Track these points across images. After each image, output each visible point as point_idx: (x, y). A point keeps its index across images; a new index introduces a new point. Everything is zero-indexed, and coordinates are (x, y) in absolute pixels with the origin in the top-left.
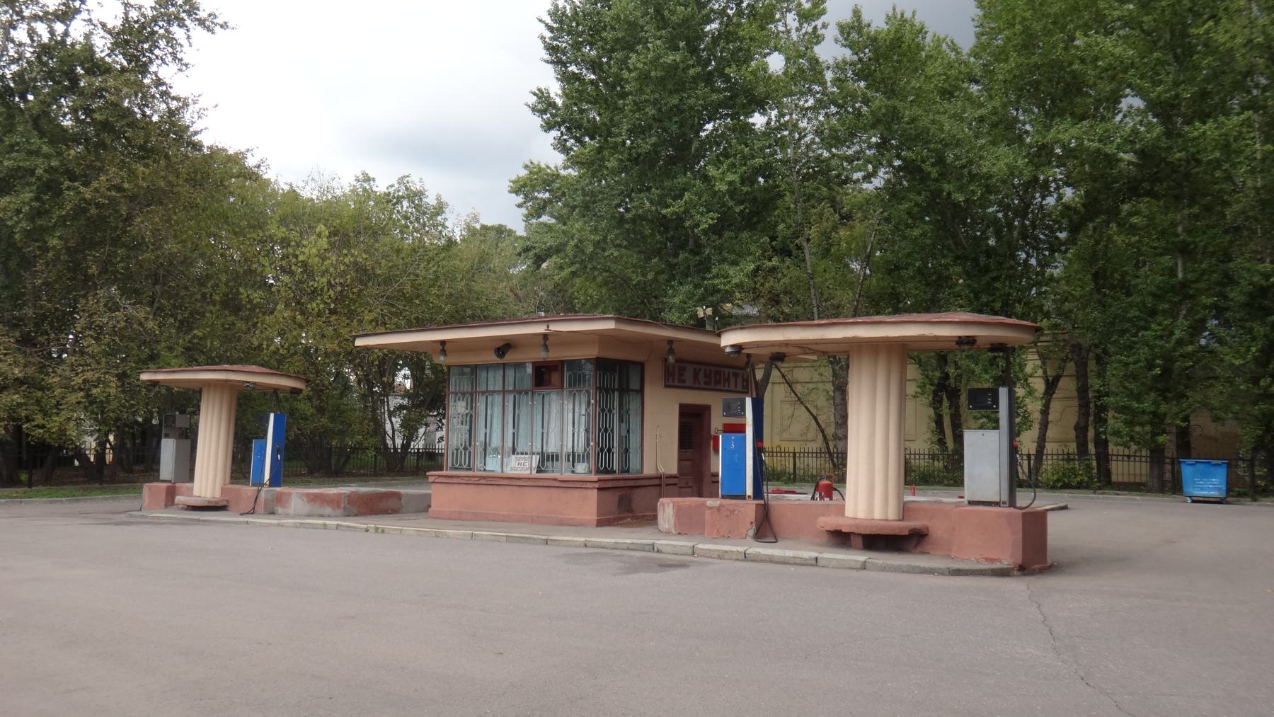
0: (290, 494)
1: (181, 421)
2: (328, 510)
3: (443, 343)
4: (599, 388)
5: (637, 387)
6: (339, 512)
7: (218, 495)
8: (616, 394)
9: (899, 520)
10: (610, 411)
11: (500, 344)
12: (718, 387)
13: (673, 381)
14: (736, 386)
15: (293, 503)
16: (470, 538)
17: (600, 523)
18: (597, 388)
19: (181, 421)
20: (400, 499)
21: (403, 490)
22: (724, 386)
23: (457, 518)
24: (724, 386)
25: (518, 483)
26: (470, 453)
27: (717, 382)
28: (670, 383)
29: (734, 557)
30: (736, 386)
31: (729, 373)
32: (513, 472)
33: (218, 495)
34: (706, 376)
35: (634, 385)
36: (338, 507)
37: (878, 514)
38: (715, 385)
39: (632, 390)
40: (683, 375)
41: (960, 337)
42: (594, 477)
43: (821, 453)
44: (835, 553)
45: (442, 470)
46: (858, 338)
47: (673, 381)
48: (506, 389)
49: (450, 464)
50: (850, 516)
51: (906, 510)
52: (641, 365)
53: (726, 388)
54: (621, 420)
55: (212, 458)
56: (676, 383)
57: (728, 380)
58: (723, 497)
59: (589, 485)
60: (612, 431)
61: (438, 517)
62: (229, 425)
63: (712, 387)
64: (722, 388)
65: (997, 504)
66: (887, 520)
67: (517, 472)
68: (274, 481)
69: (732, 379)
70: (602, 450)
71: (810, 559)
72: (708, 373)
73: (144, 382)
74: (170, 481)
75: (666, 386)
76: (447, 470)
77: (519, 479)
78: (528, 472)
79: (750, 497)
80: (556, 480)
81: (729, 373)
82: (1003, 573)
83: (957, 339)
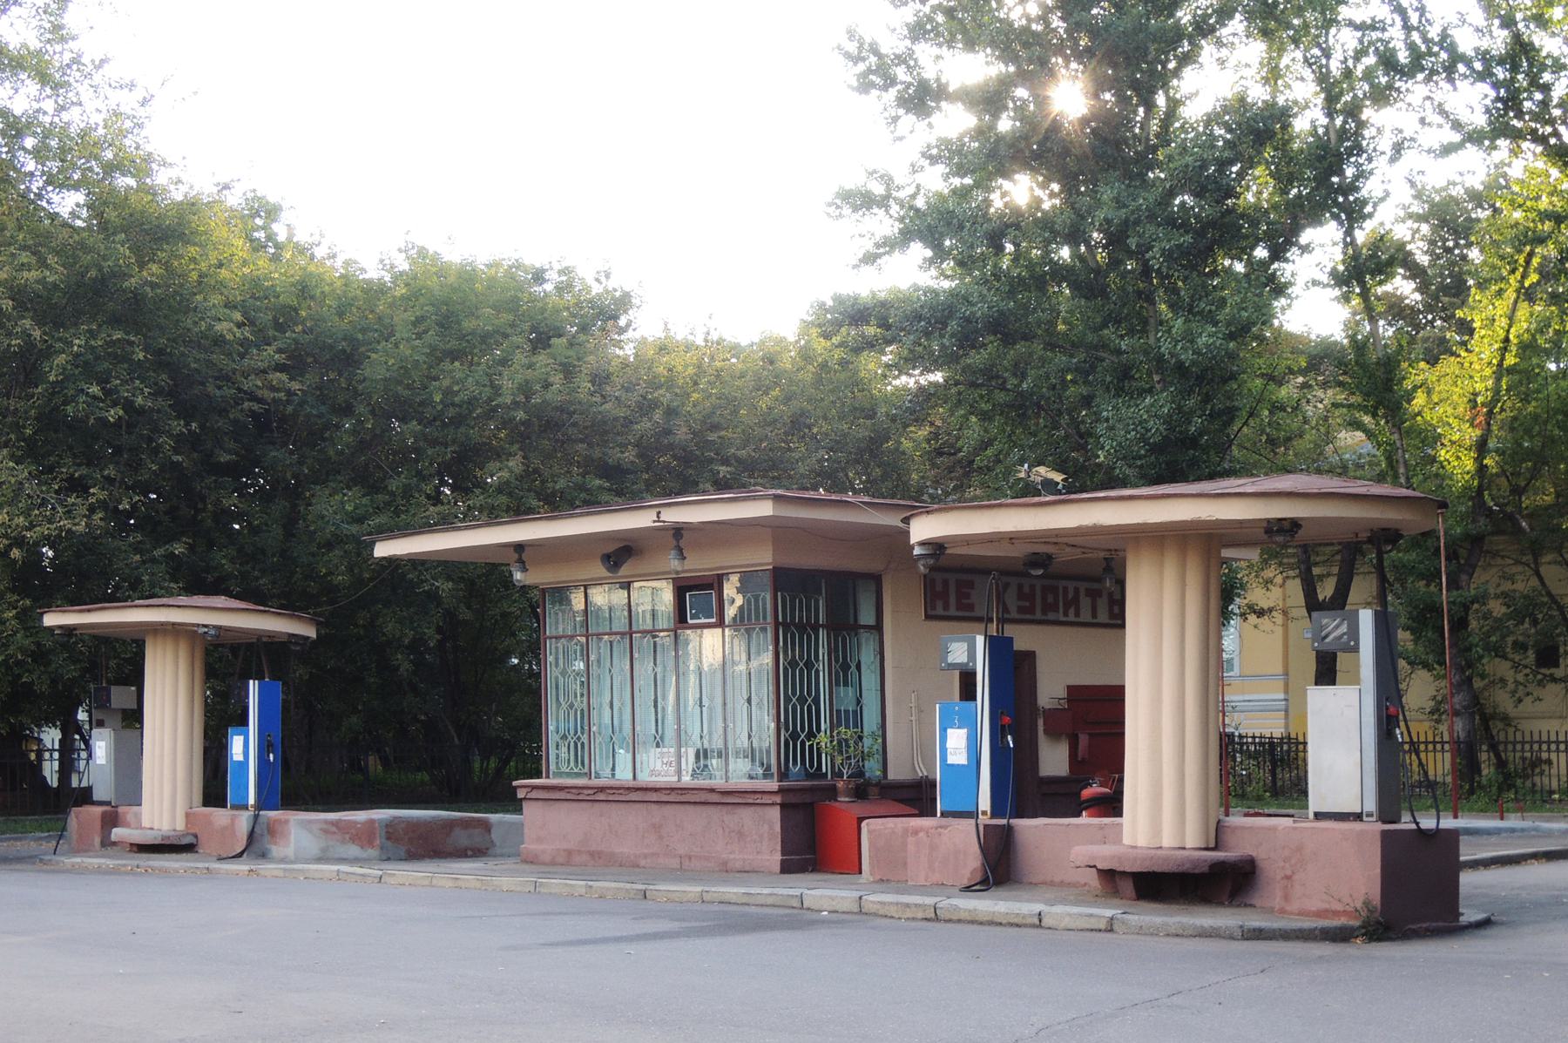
0: (287, 822)
1: (120, 697)
2: (354, 850)
3: (519, 547)
4: (786, 626)
5: (871, 621)
6: (372, 852)
7: (180, 825)
8: (822, 634)
9: (1207, 849)
10: (809, 665)
11: (611, 548)
12: (1051, 616)
13: (946, 607)
14: (1094, 615)
15: (292, 838)
16: (641, 897)
17: (787, 868)
18: (777, 624)
19: (120, 697)
20: (489, 831)
21: (494, 817)
22: (1066, 614)
23: (565, 862)
24: (1066, 614)
25: (654, 797)
26: (817, 672)
27: (1049, 607)
28: (940, 611)
29: (920, 915)
30: (1094, 615)
31: (1077, 590)
32: (654, 779)
33: (180, 825)
34: (1021, 596)
35: (867, 617)
36: (371, 843)
37: (1168, 840)
38: (1044, 612)
39: (865, 627)
40: (968, 596)
41: (1268, 521)
42: (773, 785)
43: (1434, 743)
44: (1166, 915)
45: (539, 775)
46: (1102, 526)
47: (946, 607)
48: (634, 629)
49: (552, 767)
50: (1167, 846)
51: (1219, 836)
52: (876, 579)
53: (1071, 618)
54: (834, 682)
55: (167, 761)
56: (953, 612)
57: (1075, 602)
58: (943, 814)
59: (767, 799)
60: (816, 701)
61: (531, 860)
62: (192, 701)
63: (1038, 615)
64: (1062, 618)
65: (1358, 817)
66: (1135, 847)
67: (665, 779)
68: (262, 804)
69: (1085, 602)
70: (794, 736)
71: (1031, 916)
72: (1026, 589)
73: (51, 629)
74: (108, 803)
75: (928, 617)
76: (548, 777)
77: (656, 790)
78: (675, 779)
79: (984, 813)
80: (712, 790)
81: (1077, 590)
82: (1340, 936)
83: (1265, 525)
